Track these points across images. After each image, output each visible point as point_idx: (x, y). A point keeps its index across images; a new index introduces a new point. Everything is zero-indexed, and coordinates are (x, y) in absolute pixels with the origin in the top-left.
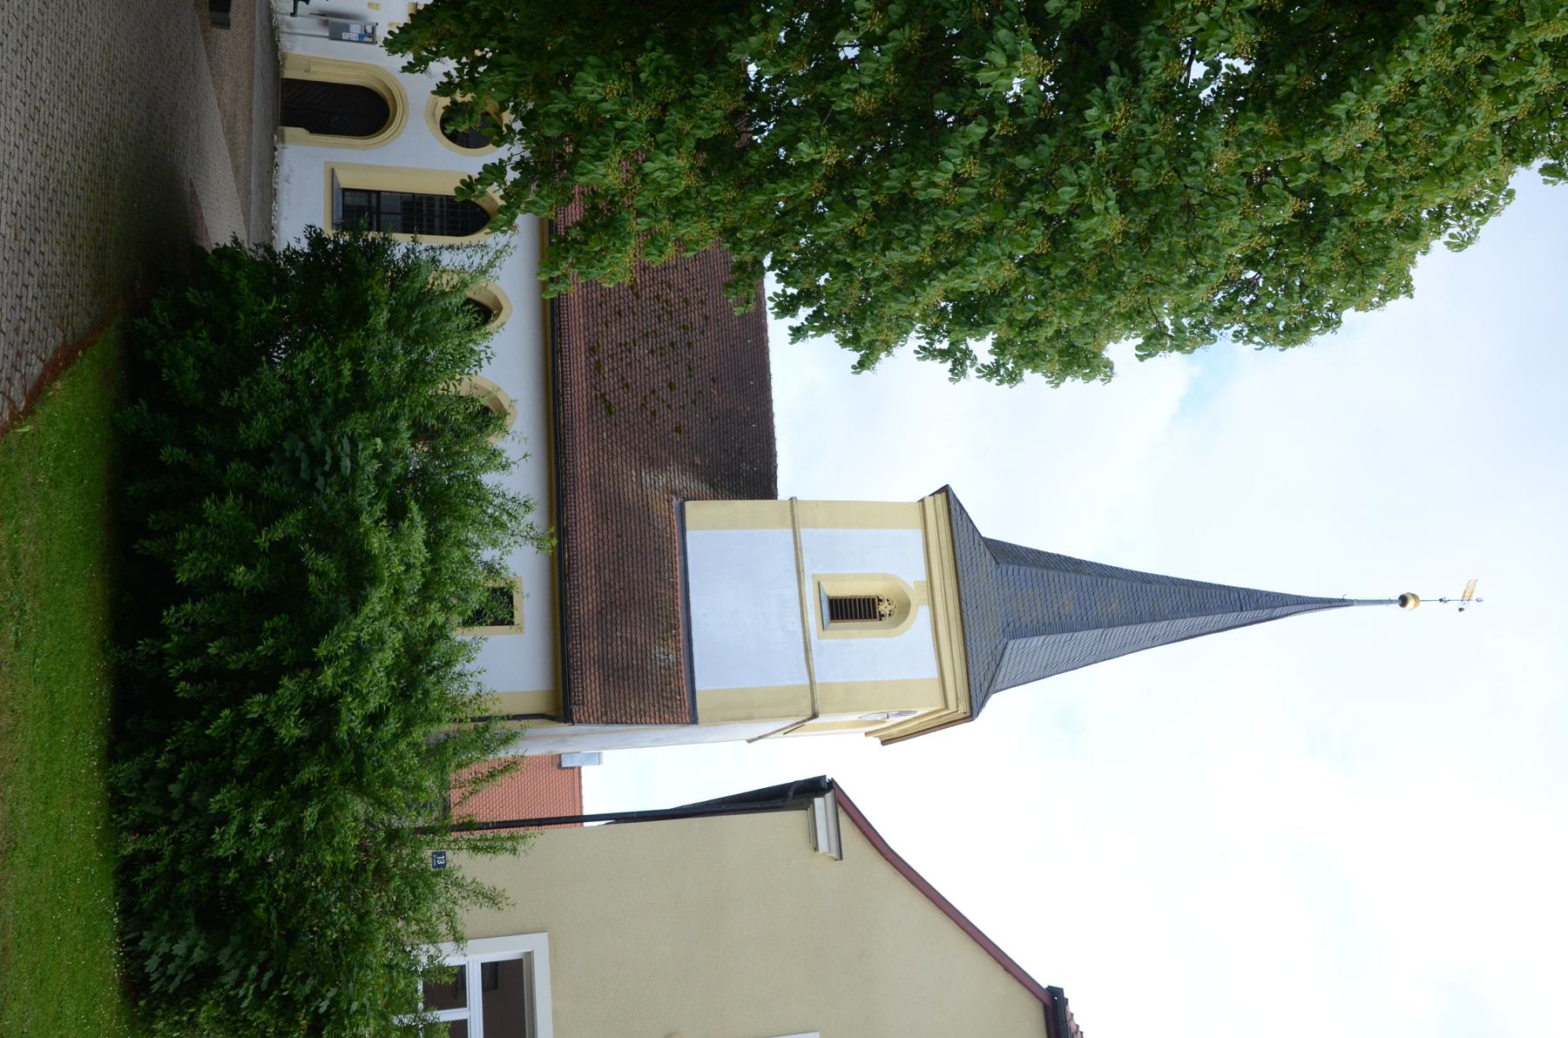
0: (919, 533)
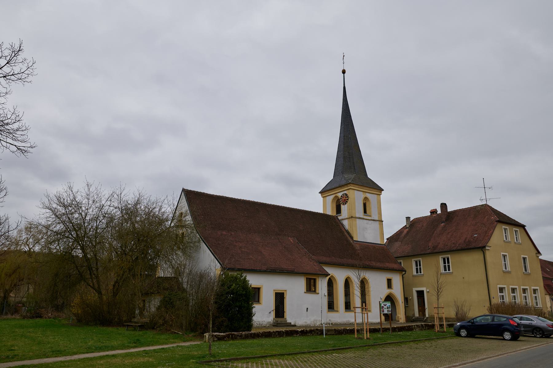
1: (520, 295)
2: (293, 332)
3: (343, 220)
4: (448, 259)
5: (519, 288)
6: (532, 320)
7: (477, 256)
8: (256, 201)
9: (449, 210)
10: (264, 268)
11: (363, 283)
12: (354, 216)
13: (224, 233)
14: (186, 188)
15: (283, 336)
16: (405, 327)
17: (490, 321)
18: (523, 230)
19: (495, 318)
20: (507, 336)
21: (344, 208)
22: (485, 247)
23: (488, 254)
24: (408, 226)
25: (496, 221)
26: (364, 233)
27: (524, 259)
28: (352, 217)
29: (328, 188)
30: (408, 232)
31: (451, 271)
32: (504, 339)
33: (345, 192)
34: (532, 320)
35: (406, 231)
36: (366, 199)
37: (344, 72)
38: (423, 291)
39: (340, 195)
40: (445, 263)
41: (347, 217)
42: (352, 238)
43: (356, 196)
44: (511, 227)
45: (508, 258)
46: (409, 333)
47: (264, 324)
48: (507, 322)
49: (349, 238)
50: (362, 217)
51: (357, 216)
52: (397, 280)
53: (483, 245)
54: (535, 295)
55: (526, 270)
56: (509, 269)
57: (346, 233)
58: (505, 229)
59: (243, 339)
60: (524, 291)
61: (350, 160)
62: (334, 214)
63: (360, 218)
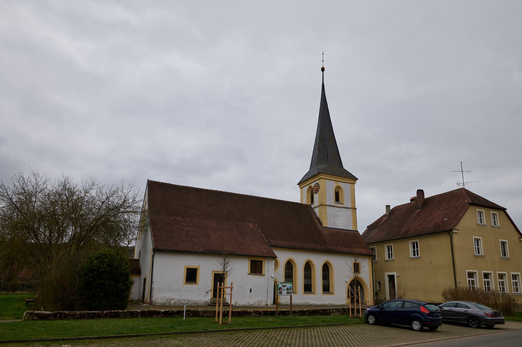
0: (327, 180)
1: (510, 281)
2: (242, 313)
3: (315, 208)
4: (417, 243)
5: (509, 274)
6: (468, 307)
7: (444, 240)
8: (233, 192)
9: (426, 196)
10: (202, 250)
11: (326, 268)
12: (323, 204)
13: (179, 218)
14: (151, 180)
15: (137, 317)
16: (318, 310)
17: (400, 306)
18: (502, 213)
19: (406, 303)
20: (416, 325)
21: (316, 196)
22: (451, 230)
23: (455, 237)
24: (387, 214)
25: (469, 204)
26: (334, 219)
27: (503, 244)
28: (322, 205)
29: (305, 179)
30: (387, 219)
31: (419, 256)
32: (412, 329)
33: (317, 182)
34: (468, 307)
35: (385, 219)
36: (338, 187)
37: (323, 69)
38: (393, 276)
39: (313, 185)
40: (414, 248)
41: (318, 205)
42: (321, 224)
43: (328, 185)
44: (488, 210)
45: (481, 243)
46: (324, 317)
47: (201, 303)
48: (416, 309)
49: (319, 225)
50: (333, 204)
51: (328, 203)
52: (365, 265)
53: (448, 228)
54: (515, 281)
55: (505, 255)
56: (482, 253)
57: (316, 221)
58: (480, 213)
59: (77, 318)
60: (501, 276)
61: (326, 154)
62: (310, 204)
63: (330, 206)
